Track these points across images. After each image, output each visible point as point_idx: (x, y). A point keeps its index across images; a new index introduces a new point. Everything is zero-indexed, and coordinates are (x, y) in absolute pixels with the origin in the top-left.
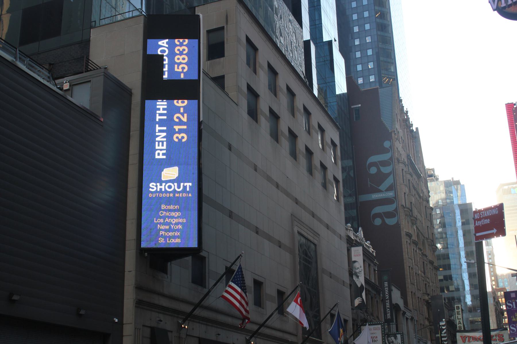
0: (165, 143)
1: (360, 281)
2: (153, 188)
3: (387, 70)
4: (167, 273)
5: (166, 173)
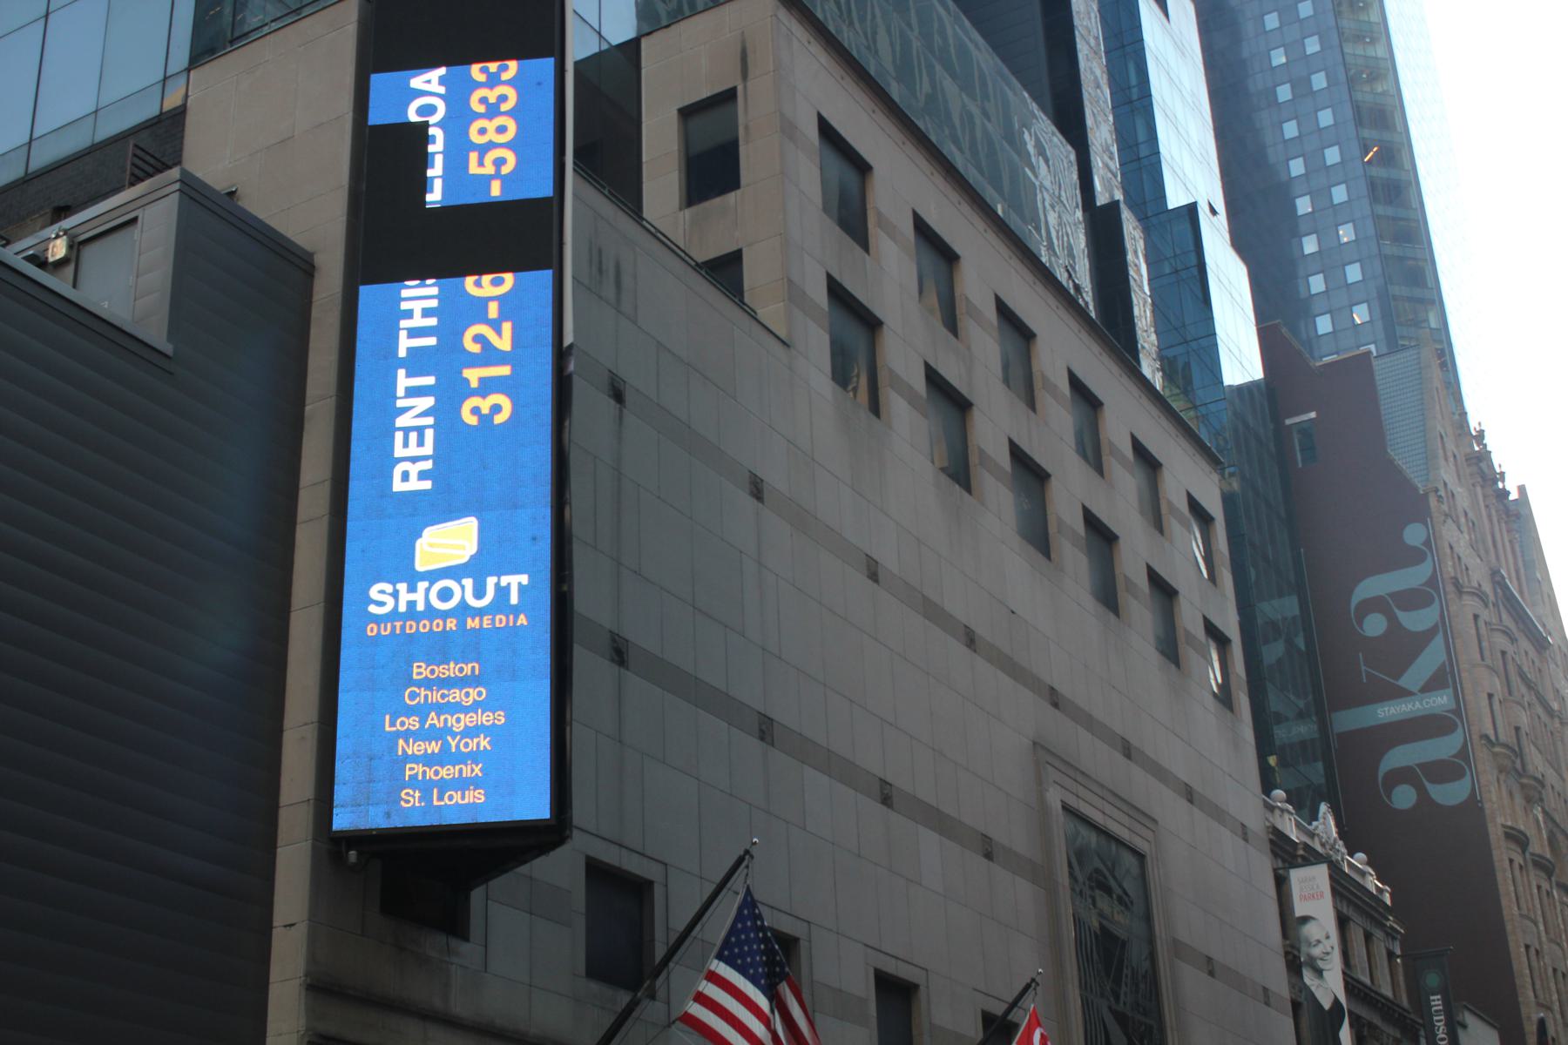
0: (429, 435)
1: (1329, 987)
2: (381, 604)
3: (1418, 323)
4: (465, 938)
5: (431, 546)
